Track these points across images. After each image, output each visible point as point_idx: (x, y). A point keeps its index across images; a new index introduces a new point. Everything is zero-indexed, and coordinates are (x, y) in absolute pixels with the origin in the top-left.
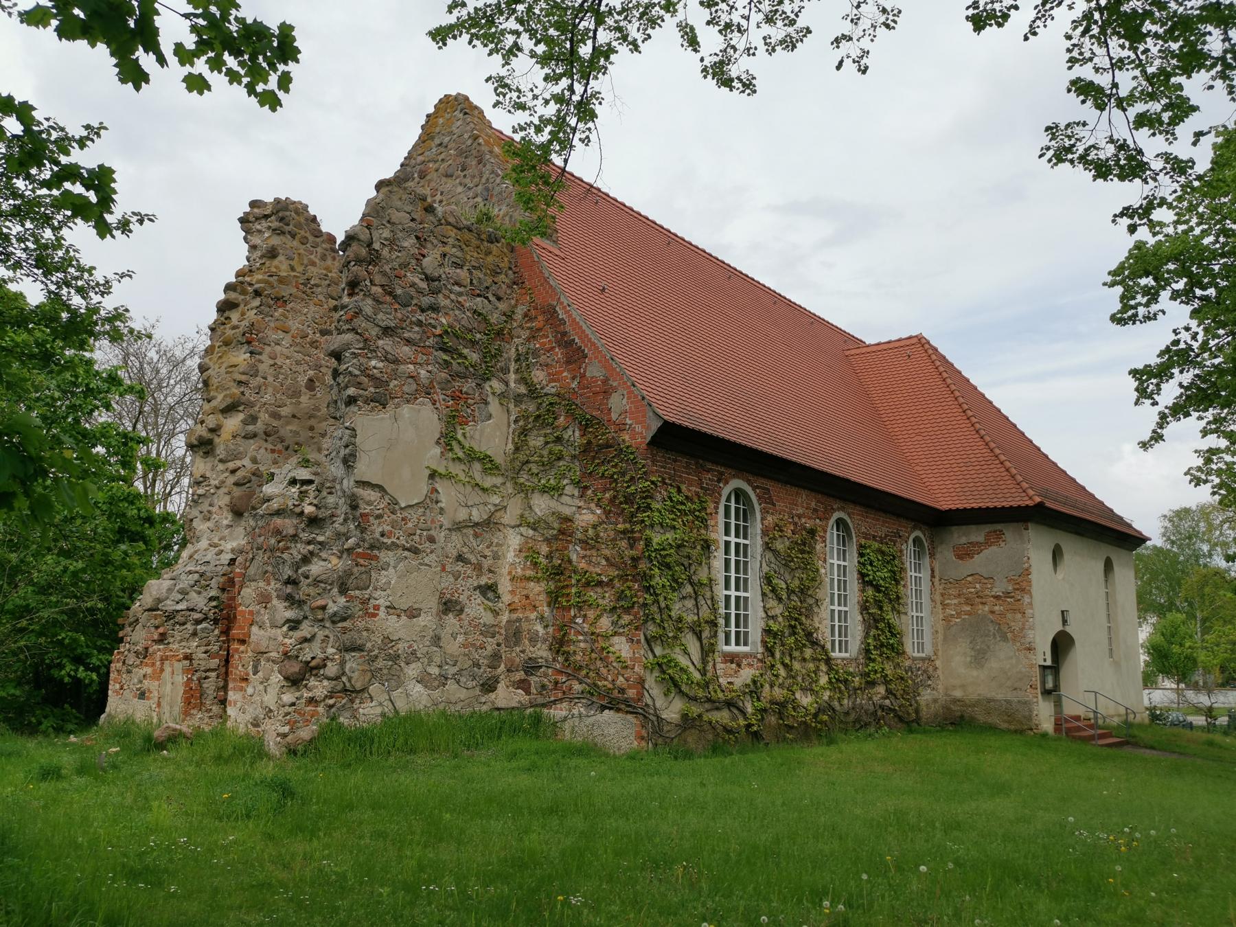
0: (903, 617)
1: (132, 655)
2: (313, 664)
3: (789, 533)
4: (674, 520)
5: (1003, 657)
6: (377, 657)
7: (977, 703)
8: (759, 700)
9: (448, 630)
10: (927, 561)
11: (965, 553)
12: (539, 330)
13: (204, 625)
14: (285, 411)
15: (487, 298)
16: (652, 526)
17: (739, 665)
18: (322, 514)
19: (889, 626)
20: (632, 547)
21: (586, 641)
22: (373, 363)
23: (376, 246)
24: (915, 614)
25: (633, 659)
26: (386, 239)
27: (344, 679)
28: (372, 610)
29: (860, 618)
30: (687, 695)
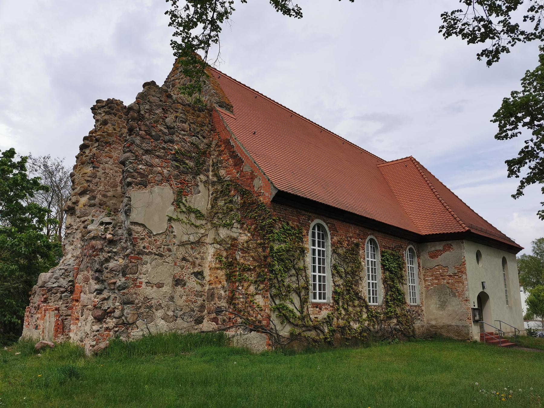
0: (405, 286)
1: (33, 309)
2: (108, 311)
3: (345, 245)
4: (285, 238)
5: (454, 305)
6: (140, 307)
7: (443, 327)
8: (331, 325)
9: (178, 293)
10: (416, 259)
11: (434, 255)
12: (223, 151)
13: (65, 294)
14: (109, 194)
15: (198, 137)
16: (274, 241)
17: (321, 309)
18: (115, 238)
19: (398, 290)
20: (264, 251)
21: (243, 298)
22: (140, 166)
23: (142, 112)
24: (411, 284)
25: (265, 306)
26: (147, 109)
27: (123, 318)
28: (138, 284)
29: (383, 286)
30: (293, 324)
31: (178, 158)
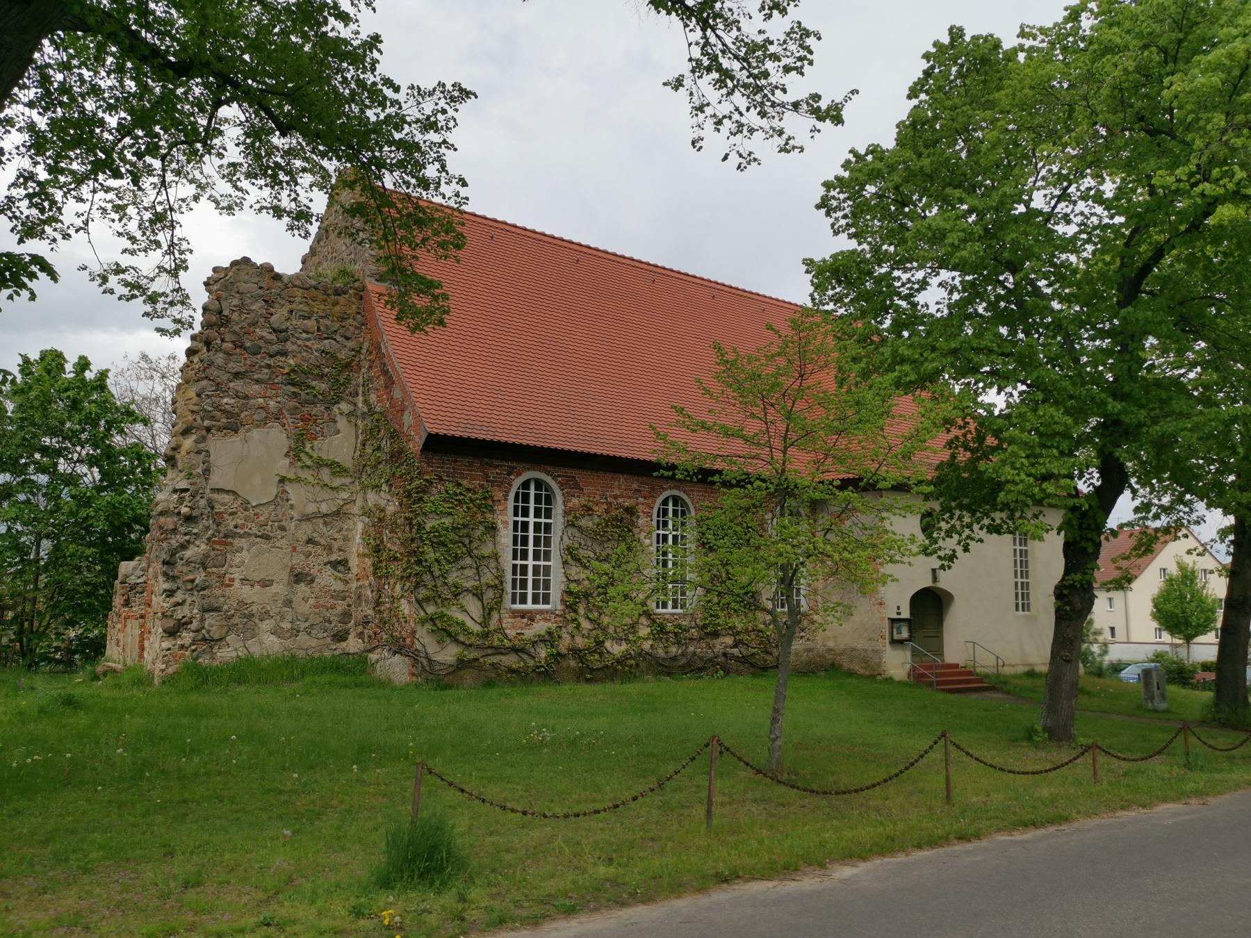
18: (195, 513)
23: (226, 313)
30: (463, 643)
31: (297, 379)
